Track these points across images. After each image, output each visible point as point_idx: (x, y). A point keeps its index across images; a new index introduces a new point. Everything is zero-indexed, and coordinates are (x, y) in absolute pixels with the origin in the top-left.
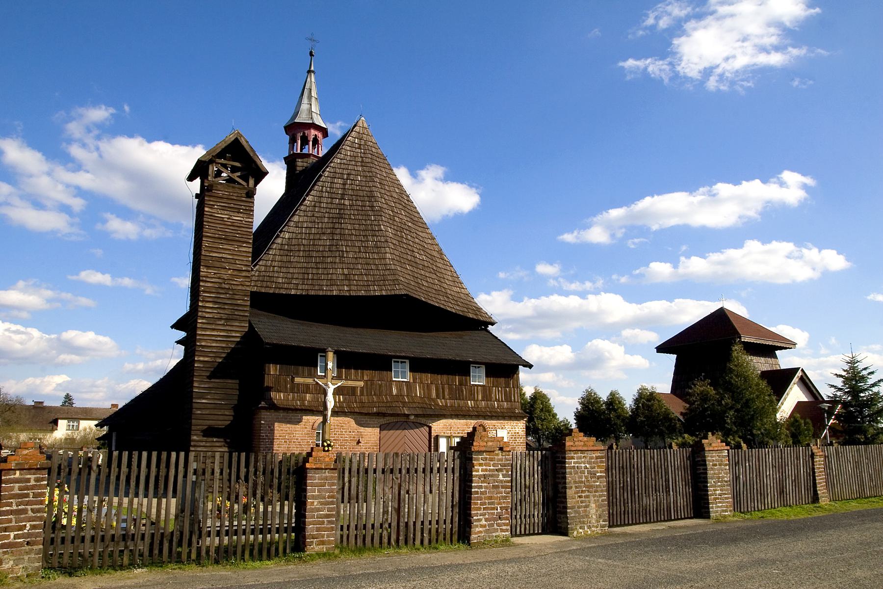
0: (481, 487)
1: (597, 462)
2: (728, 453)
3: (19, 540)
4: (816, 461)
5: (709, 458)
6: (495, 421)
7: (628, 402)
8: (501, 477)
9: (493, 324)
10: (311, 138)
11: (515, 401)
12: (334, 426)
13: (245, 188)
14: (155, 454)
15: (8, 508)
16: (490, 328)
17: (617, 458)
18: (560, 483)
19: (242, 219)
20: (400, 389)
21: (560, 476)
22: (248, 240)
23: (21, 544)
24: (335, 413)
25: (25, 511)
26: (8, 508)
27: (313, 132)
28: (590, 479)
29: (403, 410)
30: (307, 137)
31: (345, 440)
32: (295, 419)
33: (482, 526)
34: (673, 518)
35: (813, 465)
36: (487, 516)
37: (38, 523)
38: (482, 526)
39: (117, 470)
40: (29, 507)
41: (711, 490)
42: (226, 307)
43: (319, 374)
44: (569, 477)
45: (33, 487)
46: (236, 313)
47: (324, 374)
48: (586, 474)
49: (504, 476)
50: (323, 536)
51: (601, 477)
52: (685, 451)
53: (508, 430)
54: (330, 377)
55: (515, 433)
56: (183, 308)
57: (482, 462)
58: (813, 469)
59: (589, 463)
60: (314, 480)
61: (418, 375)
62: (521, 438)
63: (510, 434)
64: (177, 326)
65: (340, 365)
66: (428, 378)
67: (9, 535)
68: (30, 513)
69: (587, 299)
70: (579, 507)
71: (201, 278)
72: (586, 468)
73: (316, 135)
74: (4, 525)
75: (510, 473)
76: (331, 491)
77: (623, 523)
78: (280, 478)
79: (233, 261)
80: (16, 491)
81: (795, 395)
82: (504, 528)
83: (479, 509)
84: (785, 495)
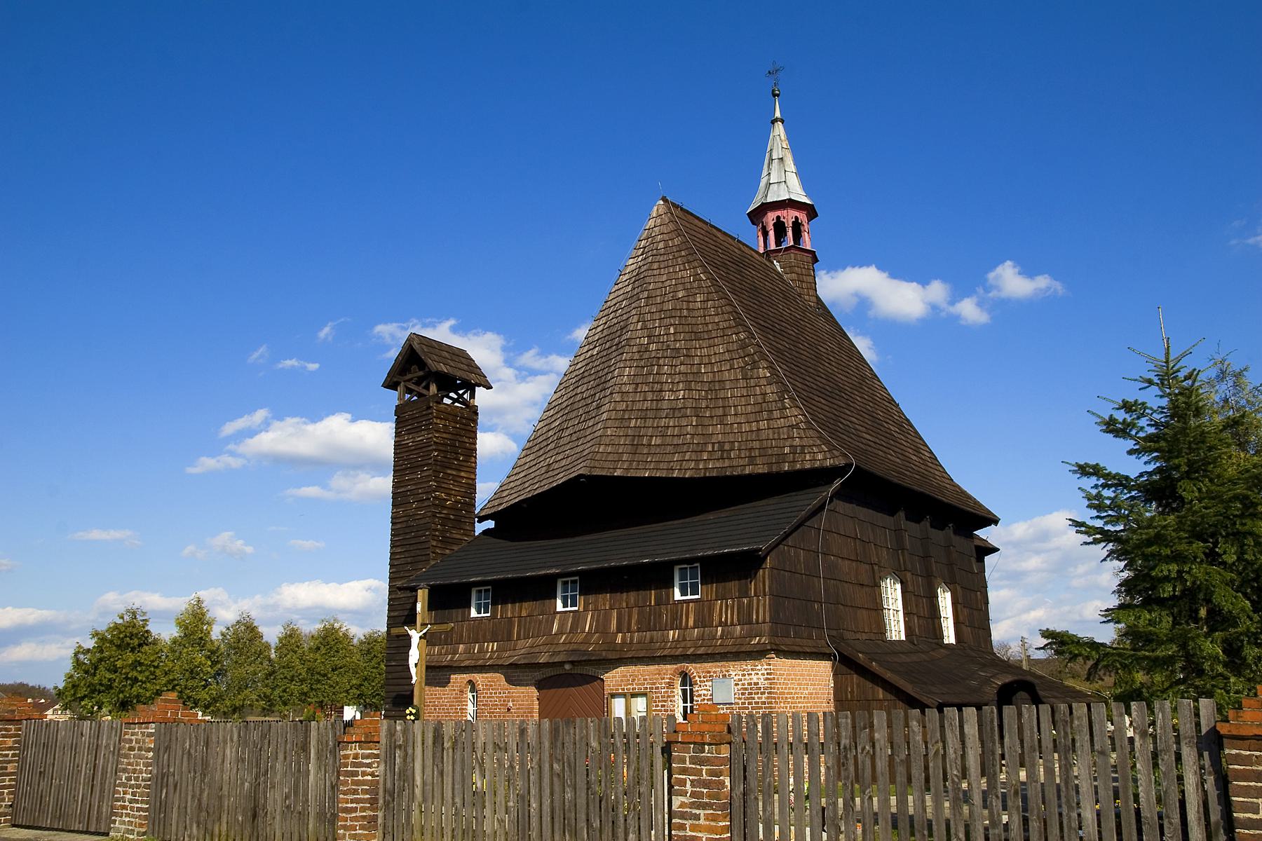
6: (710, 664)
7: (165, 632)
9: (1130, 452)
10: (789, 223)
11: (757, 623)
27: (789, 216)
53: (736, 678)
61: (591, 598)
62: (764, 693)
63: (740, 687)
65: (432, 605)
66: (605, 600)
69: (391, 384)
73: (778, 218)
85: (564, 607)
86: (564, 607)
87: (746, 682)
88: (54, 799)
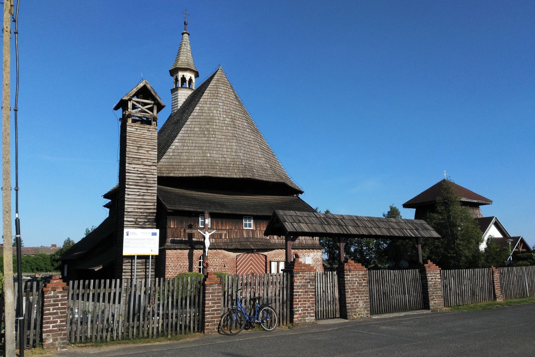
0: (298, 292)
2: (440, 272)
4: (495, 276)
5: (429, 275)
8: (309, 287)
10: (187, 79)
12: (210, 257)
15: (48, 312)
16: (300, 196)
17: (374, 275)
23: (56, 331)
24: (209, 249)
25: (57, 313)
28: (359, 287)
29: (250, 246)
31: (216, 265)
35: (493, 278)
36: (302, 308)
37: (64, 319)
40: (59, 311)
43: (200, 226)
45: (60, 300)
46: (149, 191)
47: (203, 226)
48: (357, 284)
49: (311, 285)
50: (214, 321)
51: (365, 286)
55: (316, 259)
58: (493, 281)
59: (359, 278)
64: (106, 196)
71: (127, 171)
72: (356, 280)
73: (183, 76)
74: (46, 321)
76: (219, 296)
80: (52, 302)
81: (493, 232)
83: (298, 304)
84: (475, 296)
85: (156, 235)
86: (156, 235)
87: (315, 258)
88: (492, 296)
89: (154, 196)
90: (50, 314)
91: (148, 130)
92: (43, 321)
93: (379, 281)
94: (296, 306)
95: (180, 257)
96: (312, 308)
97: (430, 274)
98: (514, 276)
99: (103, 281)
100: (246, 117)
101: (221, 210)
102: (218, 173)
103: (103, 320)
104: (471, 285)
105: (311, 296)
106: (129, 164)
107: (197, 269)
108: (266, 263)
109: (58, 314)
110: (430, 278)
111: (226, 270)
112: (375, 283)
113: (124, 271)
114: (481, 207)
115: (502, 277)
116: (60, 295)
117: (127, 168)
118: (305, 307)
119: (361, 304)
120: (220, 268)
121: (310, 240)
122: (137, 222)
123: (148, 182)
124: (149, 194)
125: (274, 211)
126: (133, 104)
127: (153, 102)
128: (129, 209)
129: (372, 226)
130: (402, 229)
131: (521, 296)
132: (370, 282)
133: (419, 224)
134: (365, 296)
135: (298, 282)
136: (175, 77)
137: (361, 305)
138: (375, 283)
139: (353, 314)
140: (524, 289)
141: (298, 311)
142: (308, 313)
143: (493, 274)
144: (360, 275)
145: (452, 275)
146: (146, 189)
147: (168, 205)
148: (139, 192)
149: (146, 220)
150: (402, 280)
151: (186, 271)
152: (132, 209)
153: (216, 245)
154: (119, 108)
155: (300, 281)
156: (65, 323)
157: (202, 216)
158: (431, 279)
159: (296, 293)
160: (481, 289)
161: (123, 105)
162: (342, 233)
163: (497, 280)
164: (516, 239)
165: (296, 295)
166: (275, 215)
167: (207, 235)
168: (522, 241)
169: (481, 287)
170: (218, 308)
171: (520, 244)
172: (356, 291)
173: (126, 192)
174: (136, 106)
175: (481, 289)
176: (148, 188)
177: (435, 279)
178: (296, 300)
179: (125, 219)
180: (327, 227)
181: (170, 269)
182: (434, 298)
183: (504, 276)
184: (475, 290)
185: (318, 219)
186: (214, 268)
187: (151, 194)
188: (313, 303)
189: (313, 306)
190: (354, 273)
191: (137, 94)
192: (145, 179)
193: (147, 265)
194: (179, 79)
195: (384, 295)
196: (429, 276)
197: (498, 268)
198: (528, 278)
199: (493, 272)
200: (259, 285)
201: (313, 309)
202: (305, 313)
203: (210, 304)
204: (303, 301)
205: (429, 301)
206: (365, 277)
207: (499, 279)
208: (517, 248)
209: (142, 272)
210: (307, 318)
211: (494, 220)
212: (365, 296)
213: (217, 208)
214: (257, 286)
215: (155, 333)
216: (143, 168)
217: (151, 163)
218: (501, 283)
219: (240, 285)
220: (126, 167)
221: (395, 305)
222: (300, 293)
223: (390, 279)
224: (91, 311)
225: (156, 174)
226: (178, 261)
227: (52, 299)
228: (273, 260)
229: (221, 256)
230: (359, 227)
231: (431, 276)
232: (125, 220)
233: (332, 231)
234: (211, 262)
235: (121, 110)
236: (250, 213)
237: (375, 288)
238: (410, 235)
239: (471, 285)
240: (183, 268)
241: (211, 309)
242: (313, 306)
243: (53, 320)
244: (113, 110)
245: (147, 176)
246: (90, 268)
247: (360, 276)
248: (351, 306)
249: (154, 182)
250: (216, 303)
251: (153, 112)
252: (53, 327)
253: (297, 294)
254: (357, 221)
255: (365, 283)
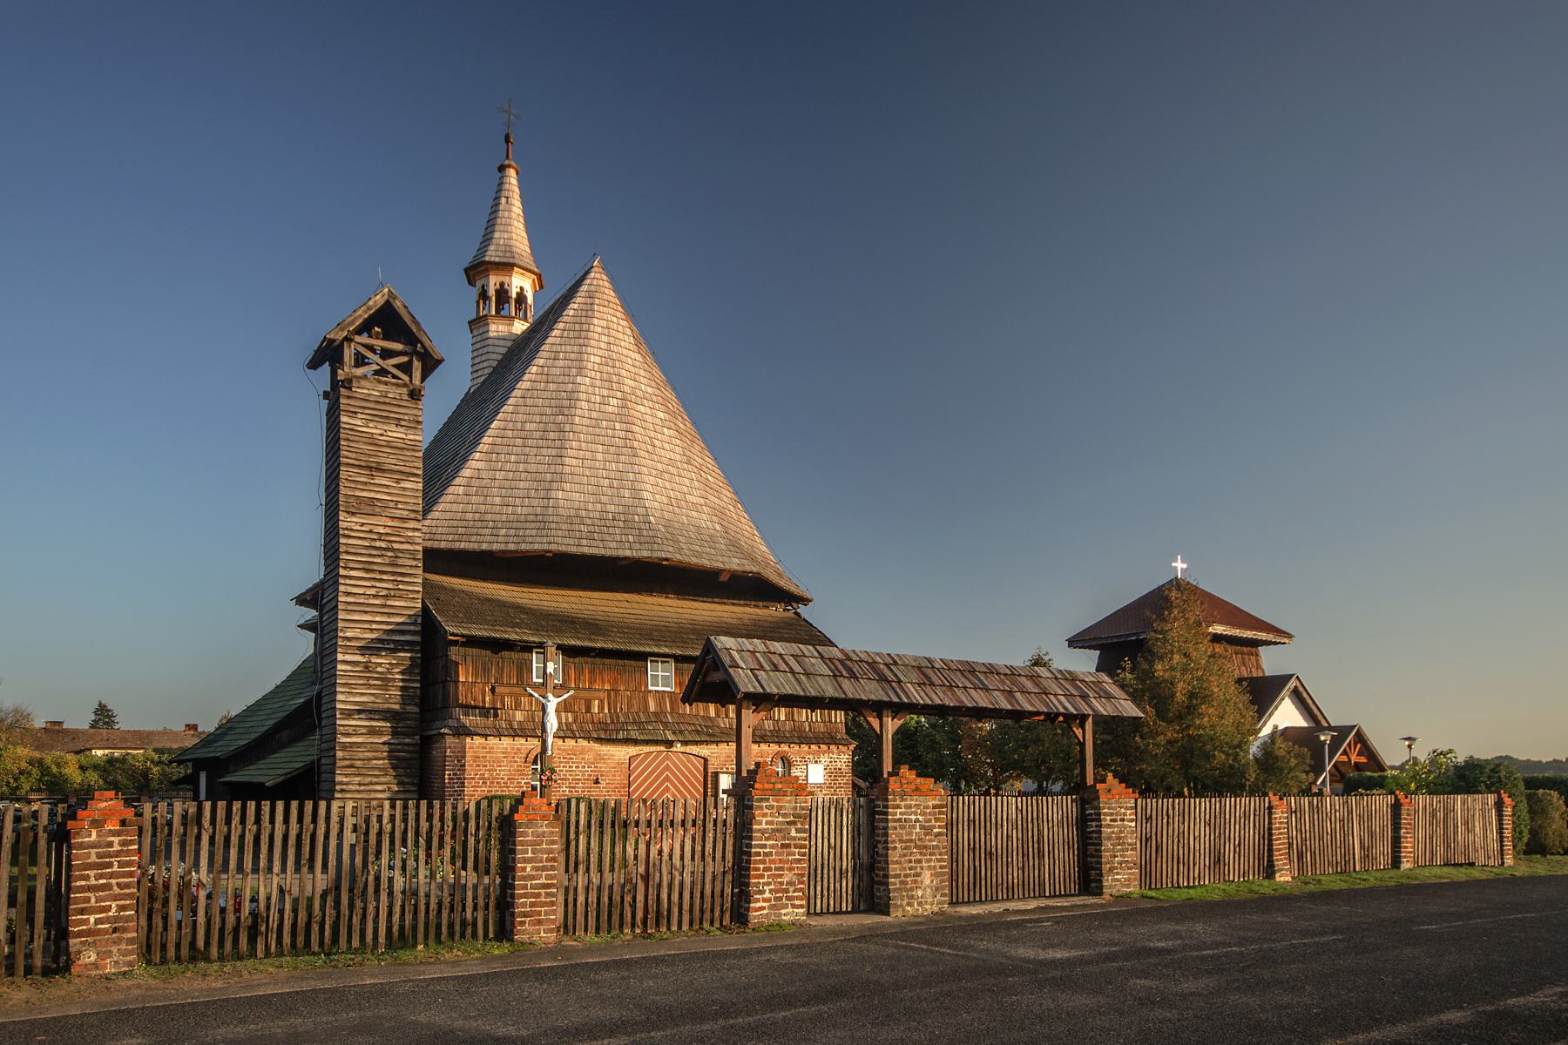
0: (764, 846)
1: (935, 813)
2: (1136, 803)
3: (103, 926)
4: (1276, 818)
5: (1106, 810)
13: (405, 385)
14: (294, 804)
15: (83, 883)
17: (966, 808)
18: (880, 842)
19: (404, 436)
20: (660, 703)
21: (880, 832)
22: (415, 471)
23: (105, 932)
25: (108, 887)
26: (83, 883)
28: (923, 836)
29: (665, 734)
30: (507, 292)
31: (575, 780)
32: (498, 748)
33: (765, 900)
34: (1047, 894)
35: (1270, 823)
36: (772, 887)
37: (128, 902)
38: (765, 900)
39: (240, 827)
40: (114, 881)
41: (1278, 865)
42: (385, 577)
43: (535, 680)
44: (892, 834)
45: (117, 854)
46: (400, 587)
47: (541, 681)
48: (918, 830)
49: (798, 831)
50: (539, 913)
51: (939, 834)
52: (1034, 802)
53: (826, 764)
54: (550, 686)
55: (835, 769)
56: (311, 572)
57: (766, 811)
59: (924, 814)
60: (526, 835)
64: (301, 600)
67: (88, 919)
68: (116, 890)
70: (906, 876)
72: (917, 821)
73: (502, 284)
74: (79, 906)
75: (807, 827)
76: (550, 851)
77: (971, 900)
78: (476, 835)
79: (392, 504)
80: (93, 859)
81: (1286, 715)
82: (797, 902)
83: (762, 876)
89: (414, 598)
90: (89, 889)
91: (397, 425)
92: (71, 907)
93: (977, 822)
94: (756, 881)
95: (483, 757)
96: (799, 886)
97: (1109, 808)
98: (1325, 819)
99: (237, 806)
100: (664, 396)
101: (591, 640)
102: (584, 542)
103: (240, 904)
104: (1212, 838)
105: (797, 857)
106: (348, 512)
107: (527, 787)
108: (705, 777)
109: (111, 889)
110: (1108, 818)
111: (602, 791)
112: (966, 828)
113: (338, 788)
114: (1261, 649)
115: (1294, 819)
116: (116, 839)
117: (341, 524)
118: (781, 883)
119: (927, 878)
120: (587, 787)
121: (822, 724)
122: (370, 664)
123: (400, 562)
124: (403, 592)
125: (708, 639)
126: (358, 354)
127: (408, 349)
128: (349, 630)
129: (969, 685)
130: (1046, 694)
131: (1339, 869)
132: (950, 825)
133: (1091, 682)
134: (938, 860)
135: (763, 821)
136: (479, 284)
137: (927, 882)
138: (966, 828)
139: (905, 903)
140: (1348, 851)
141: (763, 892)
142: (788, 898)
143: (1270, 814)
144: (928, 807)
145: (1165, 812)
146: (393, 581)
147: (450, 623)
148: (376, 587)
149: (394, 662)
150: (1035, 822)
151: (498, 791)
152: (358, 630)
153: (575, 729)
154: (321, 364)
155: (770, 819)
156: (133, 912)
157: (540, 653)
158: (1111, 820)
159: (758, 850)
160: (1237, 850)
161: (328, 354)
162: (886, 699)
163: (1280, 828)
164: (1343, 731)
165: (758, 854)
166: (709, 648)
167: (553, 703)
168: (1360, 738)
169: (1237, 843)
170: (549, 882)
171: (1352, 742)
172: (916, 847)
173: (342, 588)
174: (367, 358)
175: (1237, 850)
176: (399, 579)
177: (1122, 820)
178: (757, 865)
179: (340, 657)
180: (846, 684)
181: (456, 785)
182: (1116, 868)
183: (1298, 819)
184: (1222, 851)
185: (826, 664)
186: (570, 787)
187: (405, 592)
188: (803, 875)
189: (800, 883)
190: (913, 803)
191: (366, 328)
192: (390, 554)
193: (322, 771)
194: (492, 292)
195: (988, 857)
196: (1105, 814)
197: (1285, 798)
198: (1362, 827)
199: (1270, 808)
200: (661, 826)
201: (801, 890)
202: (781, 898)
203: (528, 869)
204: (776, 869)
205: (1101, 875)
206: (940, 813)
207: (1286, 826)
208: (1345, 752)
209: (385, 791)
210: (783, 911)
211: (1292, 684)
212: (938, 860)
213: (580, 635)
214: (655, 830)
215: (382, 940)
216: (386, 524)
217: (406, 513)
218: (1290, 834)
219: (609, 826)
220: (340, 523)
221: (1013, 882)
222: (768, 850)
223: (1005, 817)
224: (205, 882)
225: (420, 541)
226: (478, 766)
227: (93, 851)
228: (725, 770)
229: (589, 756)
230: (934, 685)
231: (1112, 814)
232: (338, 659)
233: (860, 695)
234: (562, 771)
235: (326, 367)
236: (666, 650)
237: (965, 837)
238: (1065, 708)
239: (1212, 838)
240: (491, 783)
241: (531, 884)
242: (803, 883)
243: (98, 904)
244: (306, 368)
245: (396, 546)
246: (220, 778)
247: (928, 811)
248: (901, 882)
249: (414, 563)
250: (544, 869)
251: (411, 377)
252: (97, 922)
253: (761, 850)
254: (929, 672)
255: (940, 827)
